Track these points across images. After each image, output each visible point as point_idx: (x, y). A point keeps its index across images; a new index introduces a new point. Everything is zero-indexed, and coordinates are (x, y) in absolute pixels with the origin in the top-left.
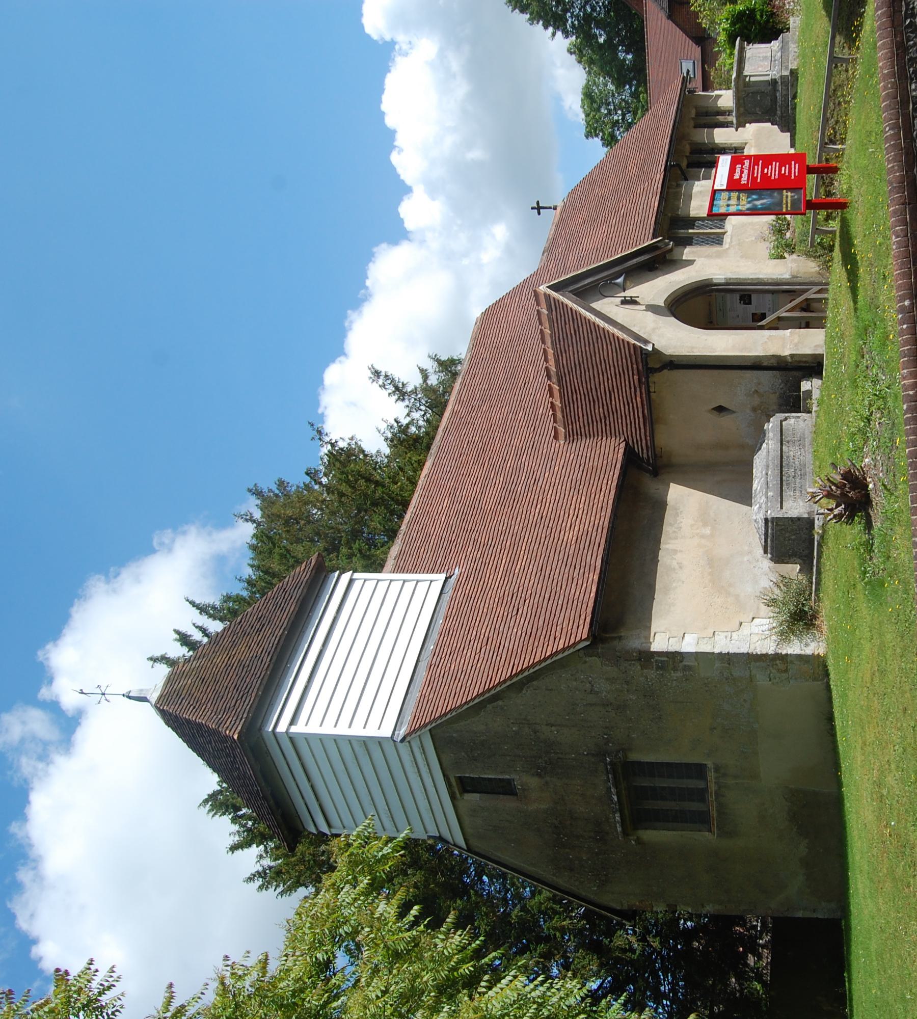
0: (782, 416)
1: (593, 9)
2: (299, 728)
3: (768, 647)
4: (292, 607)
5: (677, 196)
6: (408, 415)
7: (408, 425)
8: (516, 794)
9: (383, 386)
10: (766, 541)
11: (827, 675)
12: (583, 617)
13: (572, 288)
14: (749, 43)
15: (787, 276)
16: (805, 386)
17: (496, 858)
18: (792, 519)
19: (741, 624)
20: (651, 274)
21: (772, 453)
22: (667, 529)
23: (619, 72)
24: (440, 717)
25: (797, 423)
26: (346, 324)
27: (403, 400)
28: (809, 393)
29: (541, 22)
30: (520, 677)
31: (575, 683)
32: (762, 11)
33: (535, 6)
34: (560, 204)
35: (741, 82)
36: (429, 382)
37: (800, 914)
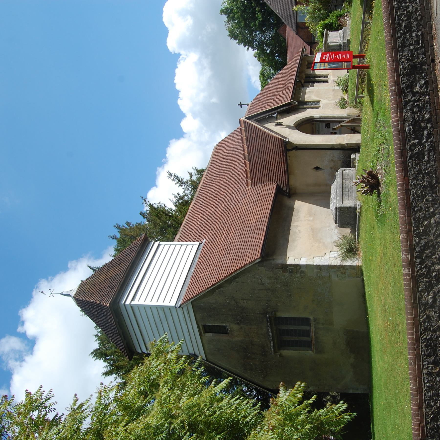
0: (344, 169)
1: (265, 38)
2: (135, 302)
3: (337, 262)
4: (133, 254)
5: (300, 93)
6: (184, 192)
7: (183, 196)
8: (228, 334)
9: (173, 180)
10: (336, 218)
11: (362, 274)
12: (258, 250)
13: (255, 119)
14: (330, 31)
15: (345, 115)
16: (353, 156)
17: (219, 365)
18: (347, 207)
19: (325, 254)
20: (288, 115)
21: (339, 183)
22: (294, 217)
23: (276, 65)
24: (196, 295)
25: (349, 171)
26: (157, 173)
27: (181, 186)
28: (354, 159)
29: (243, 44)
30: (231, 276)
31: (254, 279)
32: (335, 23)
33: (240, 37)
34: (250, 103)
35: (326, 45)
36: (193, 178)
37: (351, 391)
